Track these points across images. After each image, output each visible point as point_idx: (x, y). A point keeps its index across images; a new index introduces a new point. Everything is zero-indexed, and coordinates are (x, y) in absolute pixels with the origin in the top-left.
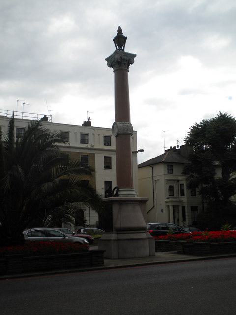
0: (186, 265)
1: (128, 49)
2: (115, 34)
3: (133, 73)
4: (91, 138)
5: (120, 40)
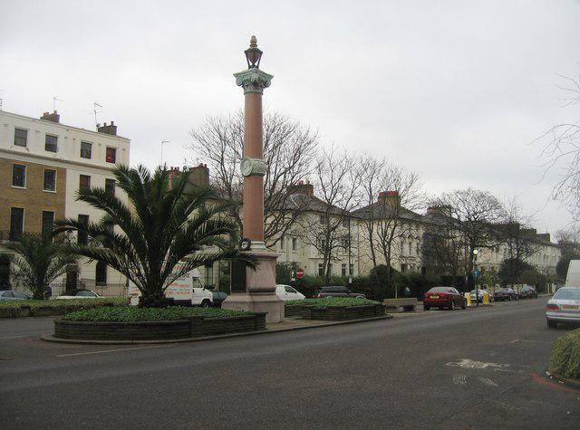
0: (326, 331)
1: (264, 66)
2: (248, 47)
3: (267, 94)
4: (60, 144)
5: (254, 54)
